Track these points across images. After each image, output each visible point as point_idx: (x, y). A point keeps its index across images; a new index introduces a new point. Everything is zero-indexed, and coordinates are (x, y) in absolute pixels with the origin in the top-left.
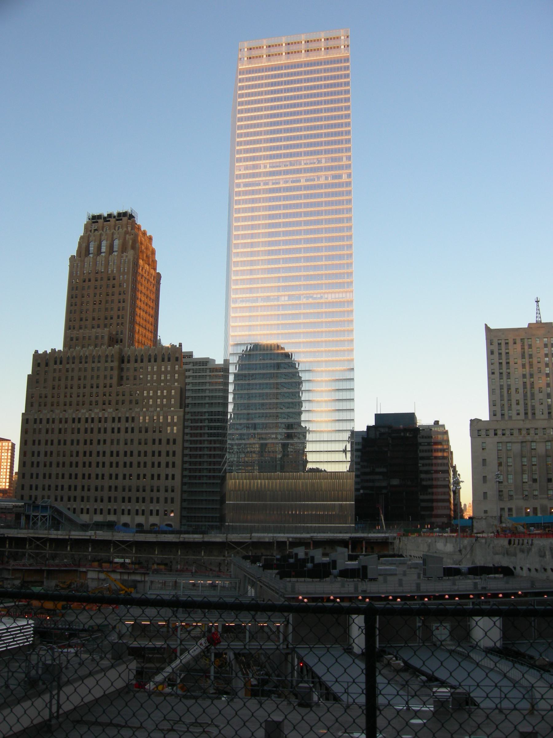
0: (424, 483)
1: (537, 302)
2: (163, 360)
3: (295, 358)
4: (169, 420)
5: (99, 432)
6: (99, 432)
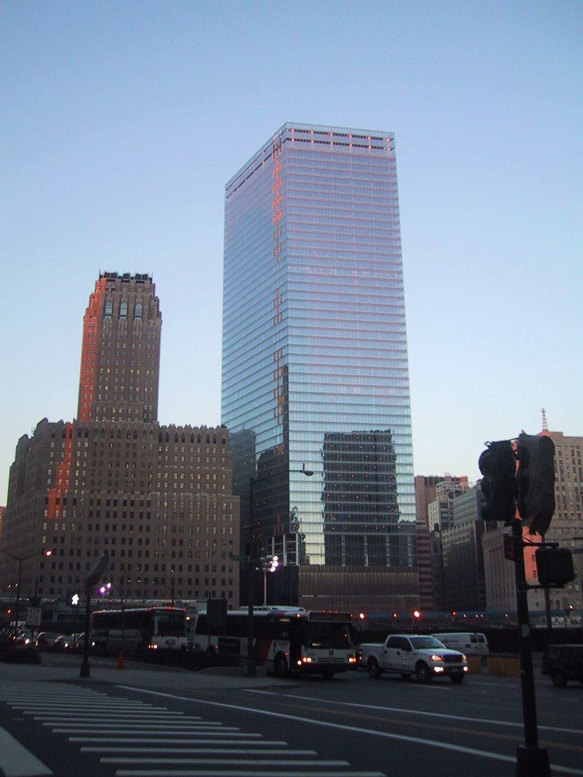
1: (543, 412)
2: (79, 435)
5: (141, 517)
6: (141, 517)
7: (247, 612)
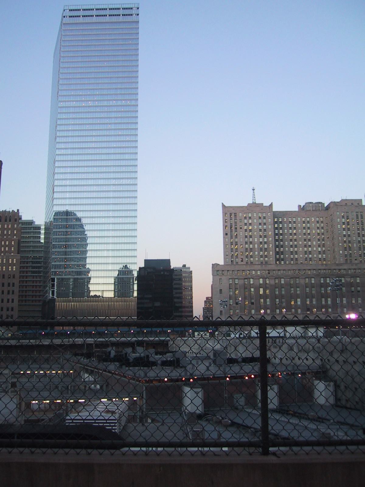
0: (177, 305)
1: (254, 190)
3: (84, 221)
4: (10, 262)
7: (221, 381)
